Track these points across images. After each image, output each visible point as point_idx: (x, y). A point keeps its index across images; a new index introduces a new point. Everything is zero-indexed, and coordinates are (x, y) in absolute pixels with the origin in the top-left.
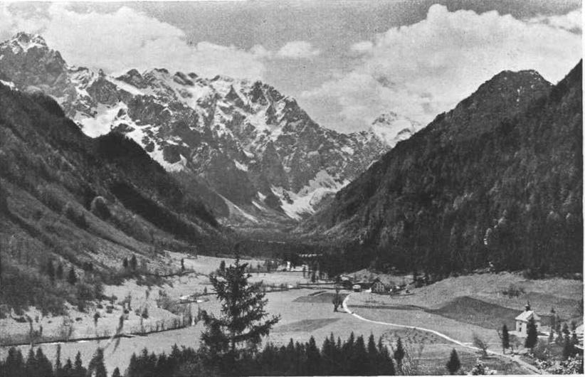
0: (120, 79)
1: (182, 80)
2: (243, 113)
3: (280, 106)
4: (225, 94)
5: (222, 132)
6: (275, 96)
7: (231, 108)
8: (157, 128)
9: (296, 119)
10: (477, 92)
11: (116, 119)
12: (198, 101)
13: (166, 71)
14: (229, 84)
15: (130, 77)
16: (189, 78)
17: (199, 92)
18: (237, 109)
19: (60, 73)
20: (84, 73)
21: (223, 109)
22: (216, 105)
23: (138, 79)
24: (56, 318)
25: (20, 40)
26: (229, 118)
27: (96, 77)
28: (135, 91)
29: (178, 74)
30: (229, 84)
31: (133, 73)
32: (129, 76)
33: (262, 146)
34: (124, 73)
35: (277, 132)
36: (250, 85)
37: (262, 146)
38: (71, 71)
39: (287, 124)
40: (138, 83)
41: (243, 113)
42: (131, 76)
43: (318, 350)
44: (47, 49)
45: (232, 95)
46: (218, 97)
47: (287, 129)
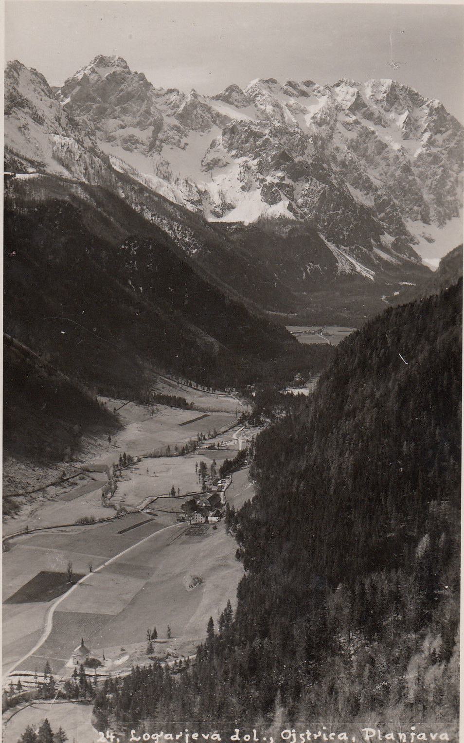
0: (217, 98)
1: (294, 92)
2: (372, 127)
3: (423, 116)
4: (349, 104)
5: (343, 156)
6: (415, 100)
7: (356, 122)
8: (256, 162)
9: (443, 129)
10: (430, 270)
11: (208, 152)
12: (314, 118)
13: (274, 81)
14: (354, 90)
15: (230, 96)
16: (304, 88)
17: (317, 106)
18: (365, 123)
19: (143, 101)
20: (173, 97)
21: (346, 125)
22: (336, 121)
23: (239, 97)
24: (288, 179)
25: (97, 66)
26: (353, 135)
27: (189, 98)
28: (235, 115)
29: (290, 84)
30: (354, 90)
31: (232, 89)
32: (228, 93)
33: (395, 170)
34: (221, 91)
35: (417, 149)
36: (384, 89)
37: (395, 170)
38: (158, 96)
39: (431, 137)
40: (239, 102)
41: (372, 127)
42: (230, 93)
43: (253, 476)
44: (129, 73)
45: (358, 105)
46: (339, 109)
47: (431, 143)
